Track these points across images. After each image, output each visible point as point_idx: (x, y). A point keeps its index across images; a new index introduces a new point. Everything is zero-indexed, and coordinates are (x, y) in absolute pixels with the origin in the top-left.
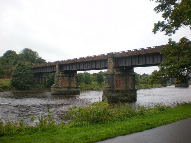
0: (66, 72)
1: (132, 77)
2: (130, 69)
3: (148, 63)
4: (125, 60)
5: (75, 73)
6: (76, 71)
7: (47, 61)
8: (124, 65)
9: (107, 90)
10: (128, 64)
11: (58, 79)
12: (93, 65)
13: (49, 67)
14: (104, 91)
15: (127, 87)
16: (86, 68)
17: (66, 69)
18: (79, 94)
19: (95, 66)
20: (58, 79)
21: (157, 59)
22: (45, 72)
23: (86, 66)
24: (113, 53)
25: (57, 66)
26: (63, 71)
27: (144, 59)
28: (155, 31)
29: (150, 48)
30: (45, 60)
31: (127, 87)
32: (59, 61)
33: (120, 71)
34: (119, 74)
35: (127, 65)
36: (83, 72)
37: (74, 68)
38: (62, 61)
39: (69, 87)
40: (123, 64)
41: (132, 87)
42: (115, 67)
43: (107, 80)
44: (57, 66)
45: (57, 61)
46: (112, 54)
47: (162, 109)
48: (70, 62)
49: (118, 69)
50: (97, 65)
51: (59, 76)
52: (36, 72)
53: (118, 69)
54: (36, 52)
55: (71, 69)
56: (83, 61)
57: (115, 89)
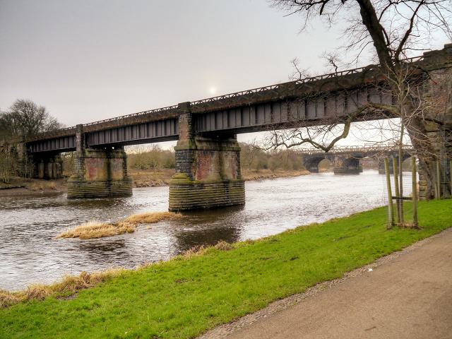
0: (99, 148)
1: (233, 153)
4: (272, 108)
5: (120, 151)
6: (120, 146)
8: (213, 129)
10: (222, 124)
11: (82, 163)
14: (172, 185)
16: (154, 137)
17: (216, 126)
18: (128, 195)
20: (82, 163)
22: (252, 125)
23: (173, 131)
24: (189, 103)
25: (78, 136)
26: (94, 147)
27: (303, 106)
32: (81, 125)
33: (206, 141)
34: (204, 148)
35: (220, 127)
36: (147, 148)
38: (88, 126)
39: (109, 181)
40: (210, 126)
41: (234, 175)
42: (193, 135)
45: (179, 104)
49: (200, 138)
50: (168, 131)
52: (38, 151)
53: (200, 138)
54: (22, 105)
55: (115, 140)
56: (261, 100)
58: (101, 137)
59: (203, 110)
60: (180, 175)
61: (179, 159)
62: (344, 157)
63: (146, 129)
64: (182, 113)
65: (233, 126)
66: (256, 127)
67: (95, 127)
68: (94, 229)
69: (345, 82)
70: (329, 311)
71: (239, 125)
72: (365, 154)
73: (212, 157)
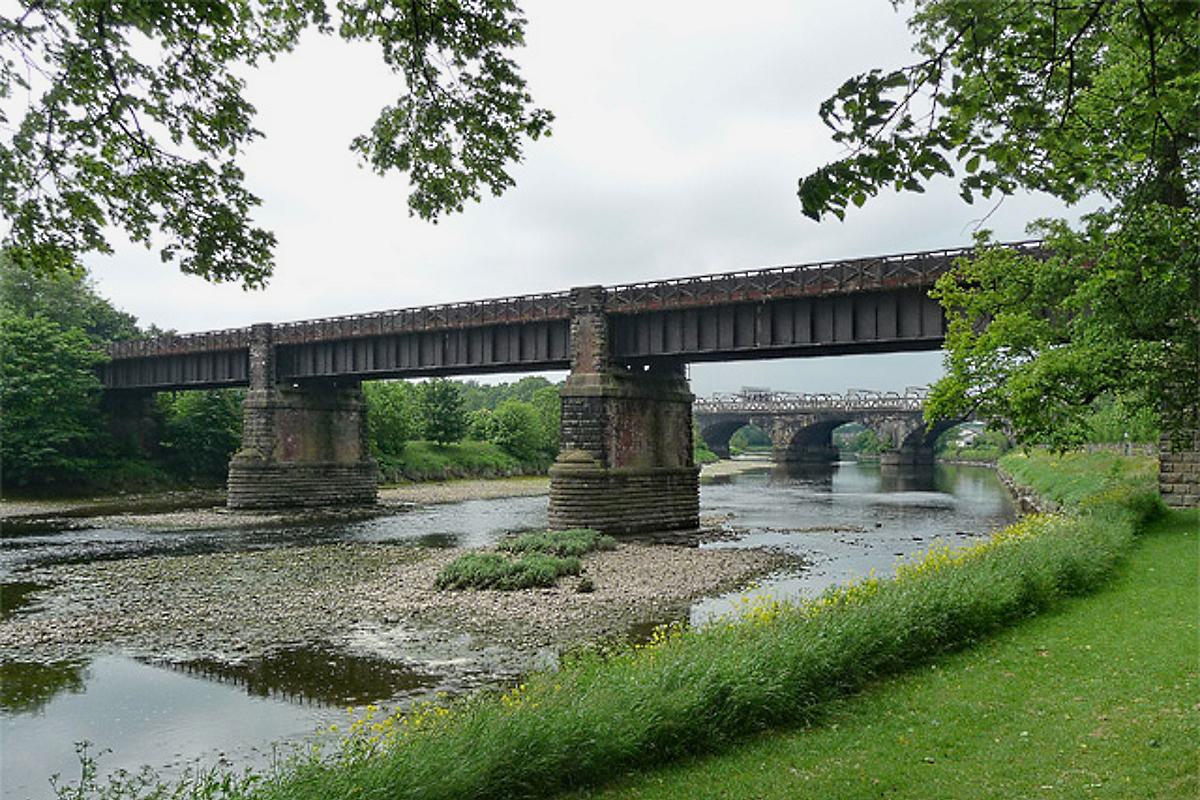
2: (671, 370)
3: (825, 340)
5: (354, 392)
6: (354, 381)
7: (143, 325)
9: (575, 477)
10: (346, 366)
12: (341, 359)
13: (155, 361)
15: (659, 459)
17: (315, 371)
19: (211, 376)
21: (718, 324)
25: (257, 353)
28: (898, 190)
29: (924, 254)
30: (133, 320)
31: (659, 459)
34: (630, 394)
37: (321, 362)
38: (632, 292)
43: (570, 425)
44: (257, 353)
46: (598, 292)
47: (156, 513)
48: (339, 333)
51: (269, 410)
57: (614, 469)
58: (174, 370)
59: (638, 306)
60: (579, 454)
61: (571, 417)
62: (798, 423)
63: (350, 353)
64: (583, 311)
65: (675, 349)
66: (520, 365)
67: (313, 333)
68: (91, 527)
69: (508, 314)
70: (558, 687)
71: (691, 346)
72: (849, 417)
73: (643, 415)
